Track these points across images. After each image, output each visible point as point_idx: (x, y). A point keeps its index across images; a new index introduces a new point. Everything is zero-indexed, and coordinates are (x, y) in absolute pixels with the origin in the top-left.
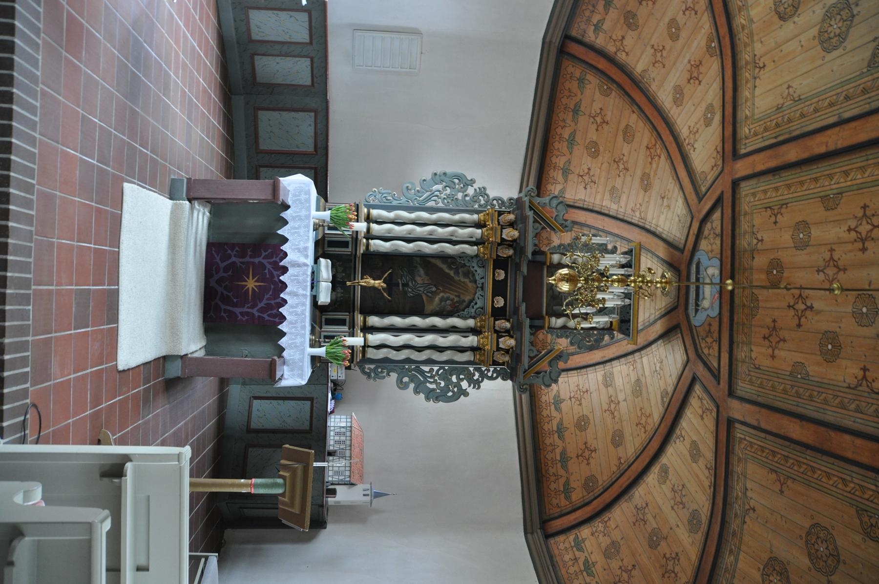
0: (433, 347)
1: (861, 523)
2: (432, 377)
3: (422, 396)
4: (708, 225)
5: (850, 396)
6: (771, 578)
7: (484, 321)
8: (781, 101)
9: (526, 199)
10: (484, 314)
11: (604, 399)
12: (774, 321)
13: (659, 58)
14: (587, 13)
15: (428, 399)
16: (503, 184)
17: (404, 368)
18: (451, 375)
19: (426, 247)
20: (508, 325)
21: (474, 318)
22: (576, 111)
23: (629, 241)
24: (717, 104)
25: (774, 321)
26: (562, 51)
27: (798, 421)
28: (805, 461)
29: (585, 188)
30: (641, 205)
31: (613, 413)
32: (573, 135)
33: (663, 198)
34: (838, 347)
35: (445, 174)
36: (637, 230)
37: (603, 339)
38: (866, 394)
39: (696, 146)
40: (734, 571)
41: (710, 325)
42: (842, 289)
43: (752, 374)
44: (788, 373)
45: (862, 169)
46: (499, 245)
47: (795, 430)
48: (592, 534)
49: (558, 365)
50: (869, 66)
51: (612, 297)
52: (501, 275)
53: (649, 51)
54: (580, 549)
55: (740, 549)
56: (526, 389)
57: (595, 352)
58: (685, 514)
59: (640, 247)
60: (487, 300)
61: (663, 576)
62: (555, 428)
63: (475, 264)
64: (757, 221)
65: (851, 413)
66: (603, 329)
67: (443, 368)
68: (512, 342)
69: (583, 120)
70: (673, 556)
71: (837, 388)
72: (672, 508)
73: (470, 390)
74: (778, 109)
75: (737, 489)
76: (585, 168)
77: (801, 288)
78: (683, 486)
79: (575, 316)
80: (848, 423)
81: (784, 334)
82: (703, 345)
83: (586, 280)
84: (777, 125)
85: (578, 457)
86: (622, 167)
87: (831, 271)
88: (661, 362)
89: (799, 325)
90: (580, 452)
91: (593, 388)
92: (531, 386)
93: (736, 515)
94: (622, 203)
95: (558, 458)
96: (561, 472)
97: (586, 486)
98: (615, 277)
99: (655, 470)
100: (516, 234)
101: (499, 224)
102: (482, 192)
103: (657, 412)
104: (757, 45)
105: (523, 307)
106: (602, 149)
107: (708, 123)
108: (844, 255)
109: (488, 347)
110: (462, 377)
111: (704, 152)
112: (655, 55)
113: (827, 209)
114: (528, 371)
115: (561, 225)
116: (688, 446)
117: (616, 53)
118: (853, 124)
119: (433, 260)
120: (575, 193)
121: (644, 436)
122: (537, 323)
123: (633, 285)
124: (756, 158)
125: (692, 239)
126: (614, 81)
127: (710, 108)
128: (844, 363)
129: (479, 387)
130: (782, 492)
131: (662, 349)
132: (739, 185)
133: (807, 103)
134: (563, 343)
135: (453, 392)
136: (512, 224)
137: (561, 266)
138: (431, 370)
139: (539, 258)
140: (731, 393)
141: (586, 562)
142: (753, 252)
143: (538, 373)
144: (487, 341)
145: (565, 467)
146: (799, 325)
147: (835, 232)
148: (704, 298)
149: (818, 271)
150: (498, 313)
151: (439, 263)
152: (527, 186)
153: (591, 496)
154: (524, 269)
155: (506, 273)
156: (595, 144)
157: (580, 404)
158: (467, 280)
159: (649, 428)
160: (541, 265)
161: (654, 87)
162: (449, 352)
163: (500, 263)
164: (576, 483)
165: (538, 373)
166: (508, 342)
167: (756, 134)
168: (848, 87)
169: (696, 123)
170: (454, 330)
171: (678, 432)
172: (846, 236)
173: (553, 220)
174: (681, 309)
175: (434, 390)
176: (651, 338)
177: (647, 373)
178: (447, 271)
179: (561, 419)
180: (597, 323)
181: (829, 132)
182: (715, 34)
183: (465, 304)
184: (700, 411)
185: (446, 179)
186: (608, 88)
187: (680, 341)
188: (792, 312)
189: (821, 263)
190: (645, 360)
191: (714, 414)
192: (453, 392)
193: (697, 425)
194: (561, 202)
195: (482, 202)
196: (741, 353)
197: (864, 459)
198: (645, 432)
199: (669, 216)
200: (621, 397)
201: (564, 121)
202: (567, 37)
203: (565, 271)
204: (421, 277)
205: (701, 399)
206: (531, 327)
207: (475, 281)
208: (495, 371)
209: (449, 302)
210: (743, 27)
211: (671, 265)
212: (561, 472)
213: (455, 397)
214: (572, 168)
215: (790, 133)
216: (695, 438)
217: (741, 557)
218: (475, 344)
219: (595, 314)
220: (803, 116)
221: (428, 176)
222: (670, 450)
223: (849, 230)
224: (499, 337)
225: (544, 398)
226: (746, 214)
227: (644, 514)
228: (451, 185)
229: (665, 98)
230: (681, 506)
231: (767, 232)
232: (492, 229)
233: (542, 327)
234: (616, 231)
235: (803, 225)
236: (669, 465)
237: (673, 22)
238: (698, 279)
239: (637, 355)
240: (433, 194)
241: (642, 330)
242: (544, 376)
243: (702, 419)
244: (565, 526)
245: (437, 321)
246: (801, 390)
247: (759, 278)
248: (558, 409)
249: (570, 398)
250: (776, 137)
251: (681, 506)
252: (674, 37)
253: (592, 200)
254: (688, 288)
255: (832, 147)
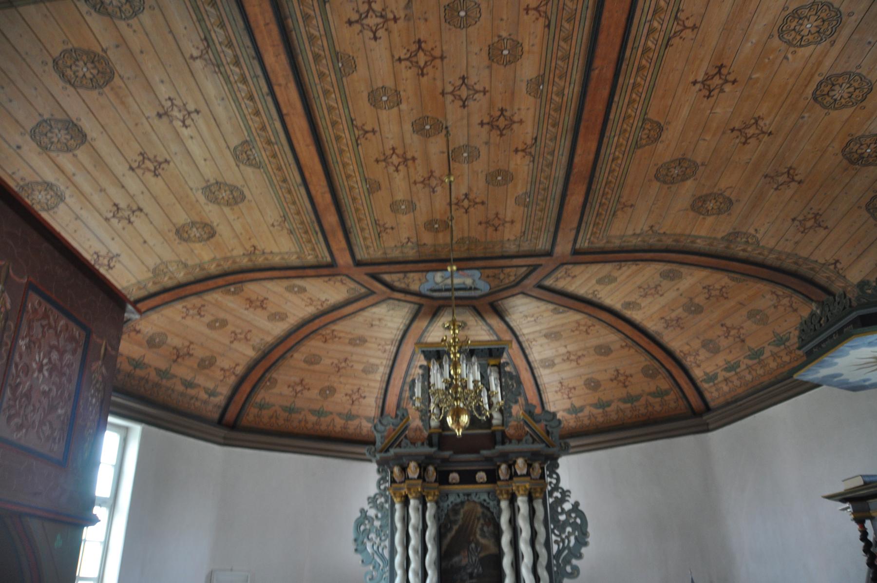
0: (533, 542)
1: (648, 144)
2: (563, 541)
3: (584, 550)
4: (397, 284)
5: (541, 160)
6: (710, 208)
7: (501, 491)
8: (285, 231)
9: (378, 456)
10: (494, 492)
11: (566, 366)
12: (480, 223)
13: (242, 336)
14: (198, 404)
15: (586, 544)
16: (364, 479)
17: (557, 572)
18: (559, 521)
19: (431, 557)
20: (503, 467)
21: (499, 502)
22: (290, 410)
23: (413, 354)
24: (286, 283)
25: (480, 223)
26: (233, 426)
27: (567, 198)
28: (602, 190)
29: (364, 397)
30: (379, 345)
31: (579, 357)
32: (313, 412)
33: (372, 325)
34: (499, 172)
35: (356, 540)
36: (404, 347)
37: (510, 373)
38: (538, 148)
39: (324, 299)
40: (710, 238)
41: (488, 277)
42: (449, 175)
43: (529, 237)
44: (526, 209)
45: (345, 165)
46: (424, 480)
47: (575, 199)
48: (699, 366)
49: (539, 414)
50: (259, 168)
51: (471, 373)
52: (454, 477)
53: (236, 345)
54: (715, 376)
55: (689, 235)
56: (565, 443)
57: (522, 378)
58: (666, 284)
59: (418, 343)
60: (480, 490)
61: (726, 298)
62: (600, 411)
63: (445, 505)
64: (392, 244)
65: (555, 159)
66: (500, 373)
67: (553, 532)
68: (520, 462)
69: (299, 403)
70: (706, 291)
71: (535, 171)
72: (661, 295)
73: (572, 500)
74: (291, 232)
75: (635, 242)
76: (345, 399)
77: (450, 204)
78: (640, 287)
79: (491, 405)
80: (564, 160)
81: (491, 215)
82: (507, 281)
83: (456, 399)
84: (306, 232)
85: (626, 387)
86: (343, 365)
87: (434, 182)
88: (526, 316)
89: (483, 203)
90: (621, 384)
91: (557, 377)
92: (563, 437)
93: (660, 241)
94: (378, 362)
95: (629, 405)
96: (643, 401)
97: (653, 376)
98: (452, 372)
99: (628, 313)
100: (413, 465)
101: (403, 482)
102: (372, 500)
103: (573, 317)
104: (235, 253)
105: (485, 453)
106: (327, 384)
107: (303, 290)
108: (419, 172)
109: (528, 486)
110: (559, 510)
111: (329, 292)
112: (240, 340)
113: (380, 188)
114: (548, 442)
115: (402, 420)
116: (602, 286)
117: (236, 376)
118: (307, 174)
119: (444, 547)
120: (370, 406)
121: (597, 327)
122: (496, 437)
123: (458, 355)
124: (334, 248)
125: (409, 298)
126: (263, 375)
127: (289, 289)
128: (512, 166)
129: (569, 491)
130: (632, 206)
131: (514, 317)
132: (359, 261)
133: (287, 210)
134: (517, 410)
135: (575, 518)
136: (404, 469)
137: (443, 422)
138: (556, 542)
139: (435, 439)
140: (549, 254)
141: (726, 370)
142: (419, 245)
143: (548, 433)
144: (521, 486)
145: (637, 398)
146: (483, 203)
147: (400, 181)
148: (464, 283)
149: (434, 192)
150: (493, 477)
151: (446, 541)
152: (364, 454)
153: (662, 370)
154: (447, 454)
155: (452, 471)
156: (322, 392)
157: (574, 388)
158: (462, 511)
159: (590, 323)
160: (442, 438)
161: (269, 339)
162: (536, 525)
163: (443, 478)
164: (651, 386)
165: (548, 433)
166: (521, 465)
167: (314, 249)
168: (275, 181)
169: (303, 300)
170: (513, 522)
171: (590, 297)
172: (383, 43)
173: (397, 428)
174: (475, 303)
175: (576, 538)
176: (505, 327)
177: (538, 328)
178: (453, 532)
179: (591, 405)
180: (496, 385)
181: (313, 192)
182: (223, 289)
183: (485, 511)
184: (569, 279)
185: (361, 538)
186: (269, 380)
187: (505, 301)
188: (472, 210)
189: (427, 190)
190: (525, 331)
191: (570, 266)
192: (575, 518)
193: (582, 281)
194: (380, 421)
195: (383, 500)
196: (512, 248)
197: (594, 146)
198: (594, 326)
199: (389, 319)
200: (563, 350)
201: (300, 422)
202: (220, 422)
203: (449, 420)
204: (462, 559)
205: (557, 280)
206: (503, 443)
207: (462, 503)
208: (550, 476)
209: (485, 529)
210: (218, 265)
211: (435, 314)
212: (643, 401)
213: (581, 515)
214: (346, 411)
215: (312, 222)
216: (594, 282)
217: (696, 234)
218: (525, 499)
219: (488, 390)
220: (298, 213)
221: (358, 558)
222: (608, 301)
223: (397, 170)
224: (516, 474)
225: (572, 423)
226: (385, 253)
227: (672, 320)
228: (367, 533)
229: (279, 329)
230: (659, 288)
231: (402, 235)
232: (409, 489)
233: (503, 432)
234: (405, 366)
235: (394, 207)
236: (622, 301)
237: (211, 326)
238: (447, 290)
239: (521, 339)
240: (377, 552)
241: (497, 336)
242: (551, 427)
243: (575, 277)
244: (695, 392)
245: (505, 540)
246: (540, 197)
247: (443, 238)
248: (581, 409)
249: (569, 398)
250: (317, 233)
251: (659, 288)
252: (224, 323)
253: (376, 391)
254: (457, 298)
255: (326, 189)
